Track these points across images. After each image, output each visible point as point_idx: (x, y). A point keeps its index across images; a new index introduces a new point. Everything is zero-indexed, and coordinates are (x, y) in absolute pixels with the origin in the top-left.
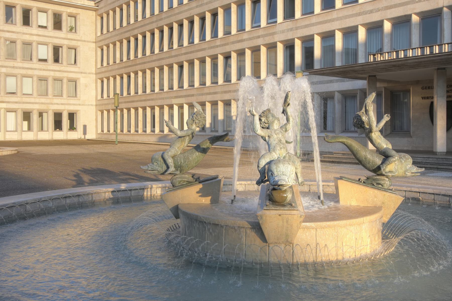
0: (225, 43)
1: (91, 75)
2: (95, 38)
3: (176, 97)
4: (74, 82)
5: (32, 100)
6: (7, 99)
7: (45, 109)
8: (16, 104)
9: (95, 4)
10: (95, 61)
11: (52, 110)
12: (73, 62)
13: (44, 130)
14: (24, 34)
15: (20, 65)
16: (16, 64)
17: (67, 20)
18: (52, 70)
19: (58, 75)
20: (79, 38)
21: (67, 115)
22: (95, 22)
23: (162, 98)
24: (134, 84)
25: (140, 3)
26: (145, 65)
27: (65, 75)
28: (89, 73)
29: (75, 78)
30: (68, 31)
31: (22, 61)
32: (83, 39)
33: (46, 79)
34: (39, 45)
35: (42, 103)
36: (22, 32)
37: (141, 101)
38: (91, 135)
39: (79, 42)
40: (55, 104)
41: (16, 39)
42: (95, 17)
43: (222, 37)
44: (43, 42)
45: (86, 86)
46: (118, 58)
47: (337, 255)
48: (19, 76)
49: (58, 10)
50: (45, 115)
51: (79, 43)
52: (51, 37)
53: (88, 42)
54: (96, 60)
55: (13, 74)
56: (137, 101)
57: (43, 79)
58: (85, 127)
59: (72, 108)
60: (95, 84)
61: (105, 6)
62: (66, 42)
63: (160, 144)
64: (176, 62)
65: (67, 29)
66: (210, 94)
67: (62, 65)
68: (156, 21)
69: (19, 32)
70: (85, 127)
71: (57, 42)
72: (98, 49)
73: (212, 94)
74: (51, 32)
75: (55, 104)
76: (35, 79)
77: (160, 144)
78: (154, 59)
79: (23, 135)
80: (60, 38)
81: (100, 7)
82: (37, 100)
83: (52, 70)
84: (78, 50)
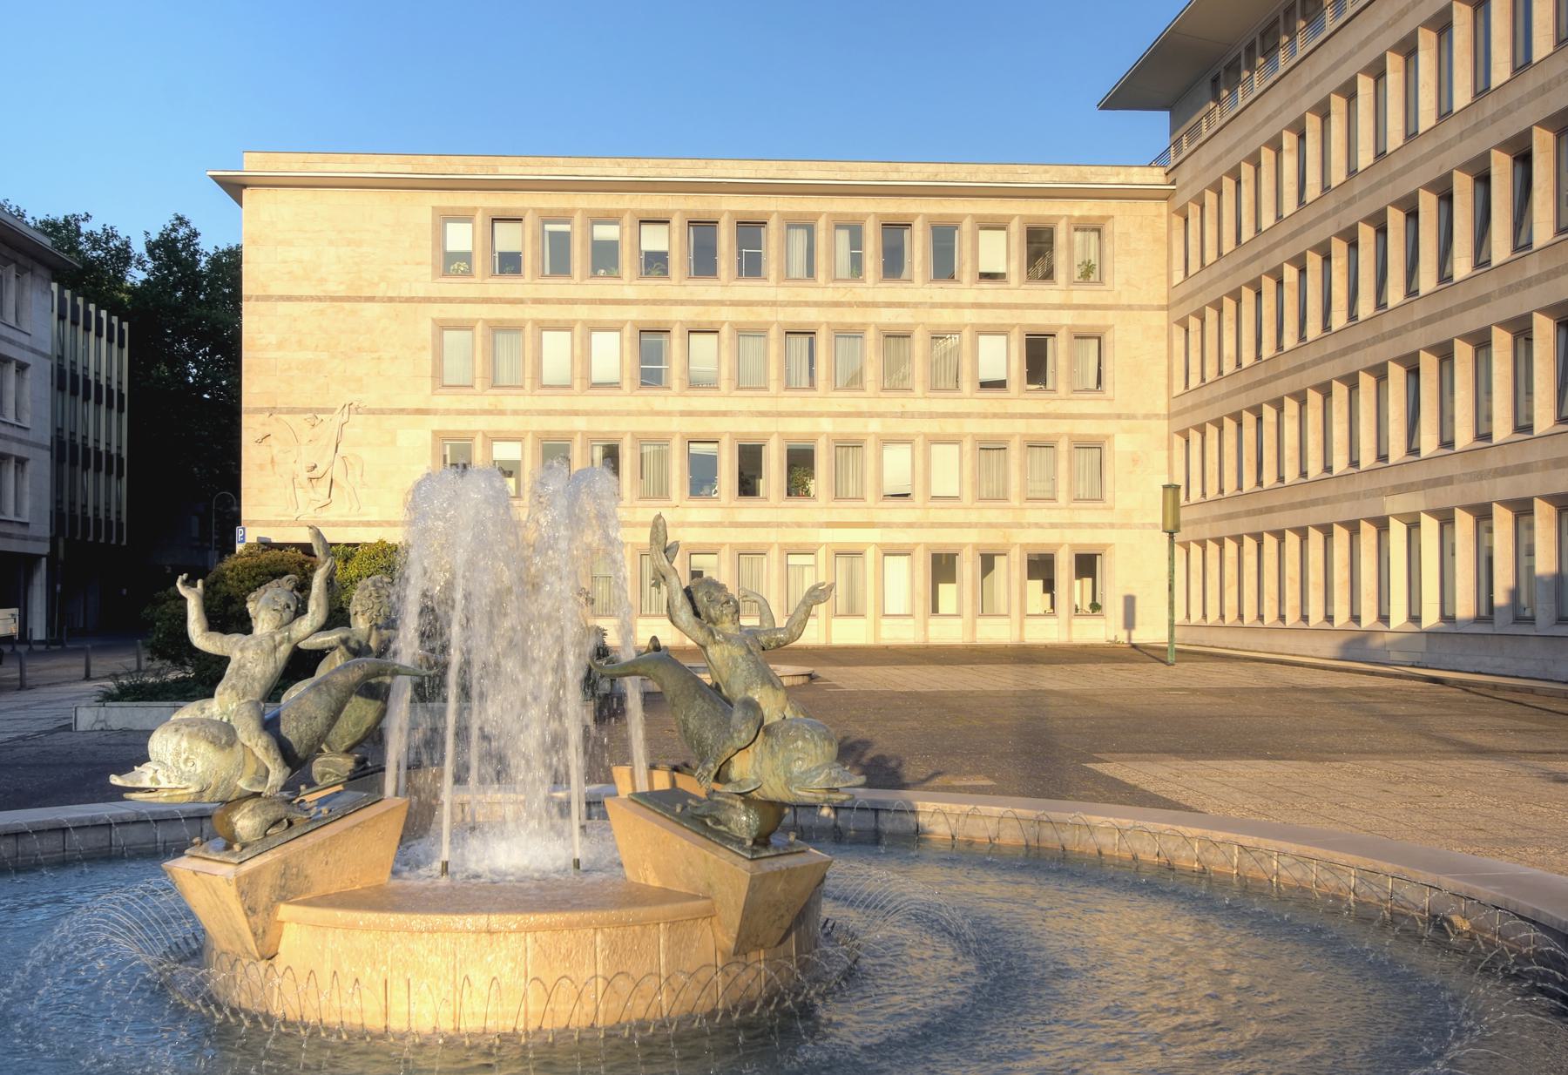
0: (1557, 268)
1: (1154, 423)
2: (1165, 293)
3: (1399, 489)
4: (1094, 446)
5: (958, 516)
6: (883, 516)
7: (998, 544)
8: (909, 530)
9: (1167, 174)
10: (1165, 372)
11: (1021, 545)
12: (1092, 383)
13: (941, 612)
14: (933, 305)
15: (923, 405)
16: (913, 405)
17: (1070, 244)
18: (1022, 416)
19: (1040, 428)
20: (1110, 301)
21: (1070, 562)
22: (1165, 239)
23: (1353, 494)
24: (1275, 445)
25: (1290, 150)
26: (1305, 374)
27: (1064, 427)
28: (1147, 417)
29: (1098, 436)
30: (1076, 279)
31: (928, 394)
32: (1124, 301)
33: (1003, 446)
34: (982, 339)
35: (990, 525)
36: (929, 300)
37: (1293, 506)
38: (1151, 631)
39: (1110, 313)
40: (1029, 525)
41: (911, 324)
42: (1164, 220)
43: (1551, 243)
44: (995, 325)
45: (1135, 461)
46: (1228, 357)
47: (456, 1017)
48: (919, 441)
49: (1040, 217)
50: (999, 562)
51: (1110, 317)
52: (1016, 306)
53: (1142, 308)
54: (1170, 368)
55: (902, 435)
56: (1282, 508)
57: (992, 447)
58: (1130, 602)
59: (1086, 539)
60: (1165, 453)
61: (1194, 178)
62: (1066, 318)
63: (1348, 670)
64: (1398, 354)
65: (1070, 275)
66: (1504, 472)
67: (1052, 395)
68: (1336, 210)
69: (921, 303)
70: (1130, 602)
71: (1038, 320)
72: (1175, 326)
73: (1513, 474)
74: (1018, 290)
75: (1029, 525)
76: (967, 445)
77: (1348, 670)
78: (1329, 351)
79: (930, 628)
80: (1045, 307)
82: (973, 517)
83: (1022, 416)
84: (1107, 339)
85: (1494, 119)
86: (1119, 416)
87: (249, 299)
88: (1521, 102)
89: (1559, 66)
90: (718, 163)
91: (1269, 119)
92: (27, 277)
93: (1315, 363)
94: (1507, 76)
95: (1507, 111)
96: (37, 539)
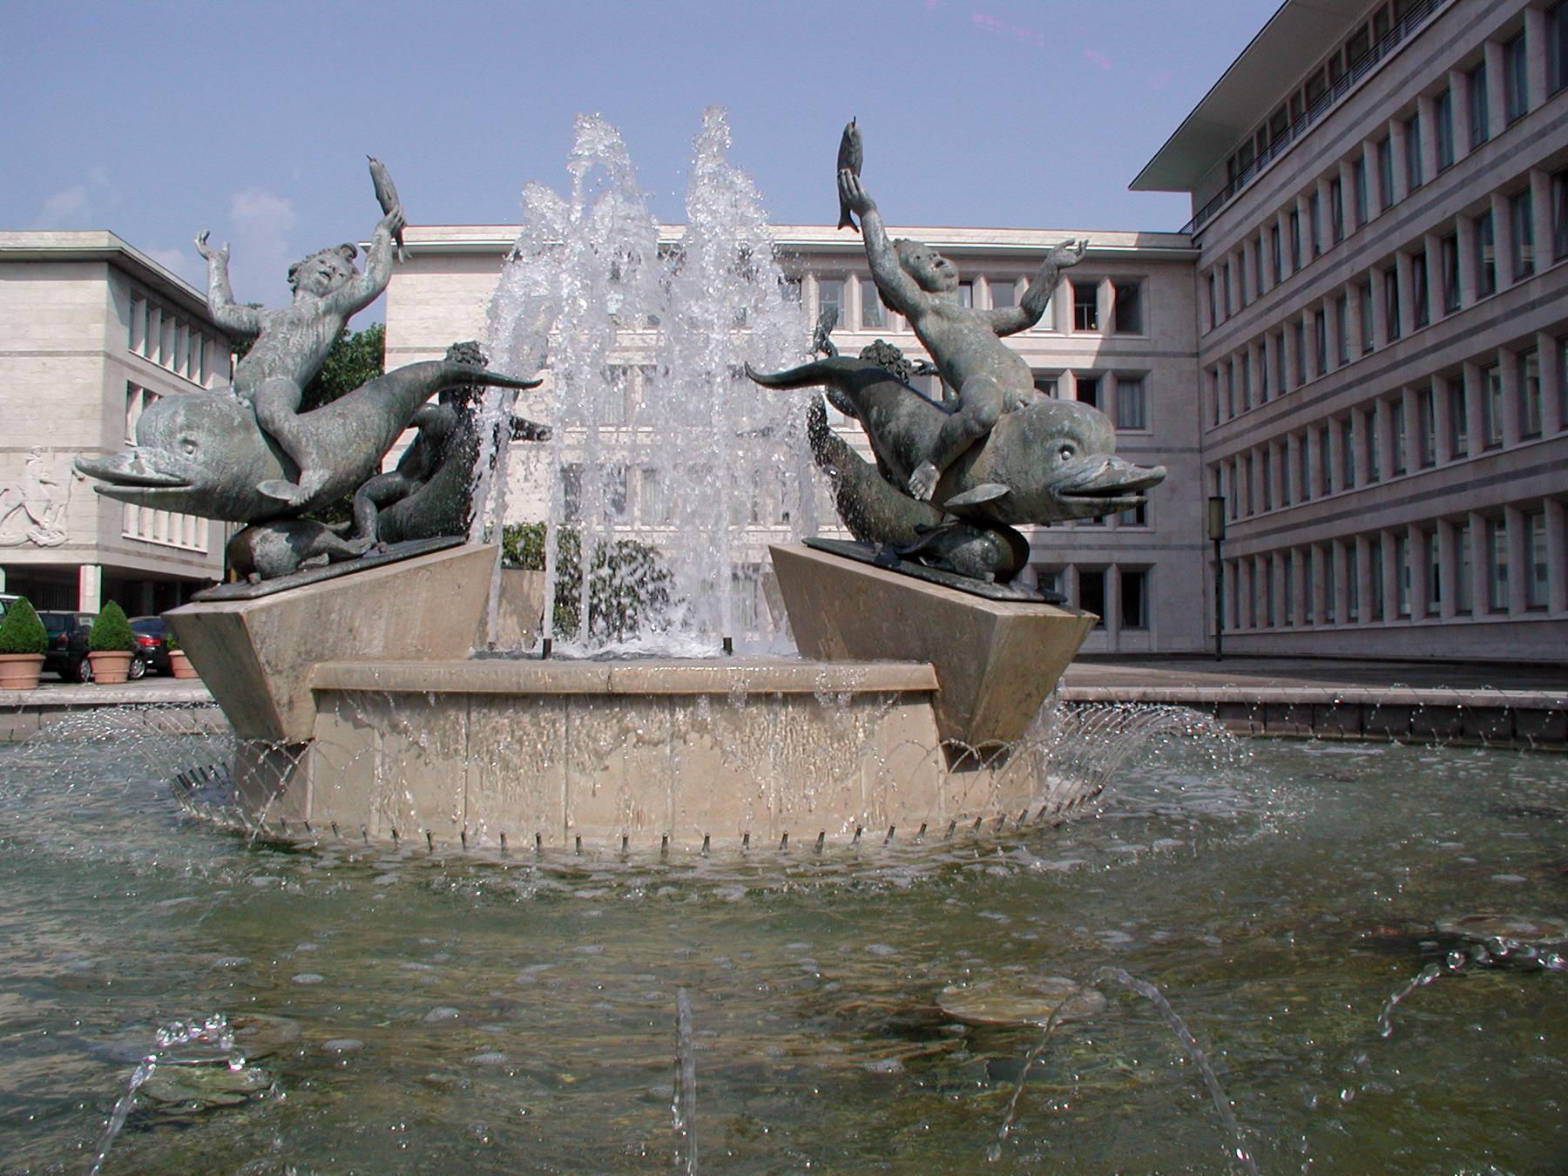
40: (1081, 547)
81: (1204, 247)
85: (1494, 165)
86: (1158, 450)
87: (391, 350)
88: (1518, 148)
89: (1555, 112)
90: (801, 228)
91: (1283, 186)
92: (211, 344)
93: (1335, 393)
94: (1502, 129)
95: (1505, 157)
96: (214, 567)
